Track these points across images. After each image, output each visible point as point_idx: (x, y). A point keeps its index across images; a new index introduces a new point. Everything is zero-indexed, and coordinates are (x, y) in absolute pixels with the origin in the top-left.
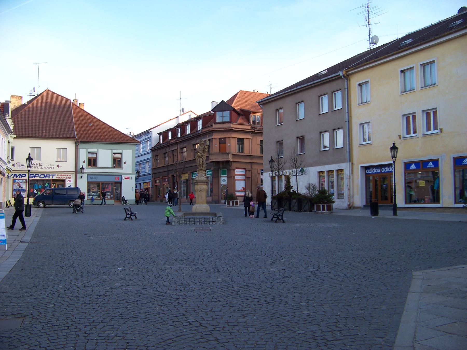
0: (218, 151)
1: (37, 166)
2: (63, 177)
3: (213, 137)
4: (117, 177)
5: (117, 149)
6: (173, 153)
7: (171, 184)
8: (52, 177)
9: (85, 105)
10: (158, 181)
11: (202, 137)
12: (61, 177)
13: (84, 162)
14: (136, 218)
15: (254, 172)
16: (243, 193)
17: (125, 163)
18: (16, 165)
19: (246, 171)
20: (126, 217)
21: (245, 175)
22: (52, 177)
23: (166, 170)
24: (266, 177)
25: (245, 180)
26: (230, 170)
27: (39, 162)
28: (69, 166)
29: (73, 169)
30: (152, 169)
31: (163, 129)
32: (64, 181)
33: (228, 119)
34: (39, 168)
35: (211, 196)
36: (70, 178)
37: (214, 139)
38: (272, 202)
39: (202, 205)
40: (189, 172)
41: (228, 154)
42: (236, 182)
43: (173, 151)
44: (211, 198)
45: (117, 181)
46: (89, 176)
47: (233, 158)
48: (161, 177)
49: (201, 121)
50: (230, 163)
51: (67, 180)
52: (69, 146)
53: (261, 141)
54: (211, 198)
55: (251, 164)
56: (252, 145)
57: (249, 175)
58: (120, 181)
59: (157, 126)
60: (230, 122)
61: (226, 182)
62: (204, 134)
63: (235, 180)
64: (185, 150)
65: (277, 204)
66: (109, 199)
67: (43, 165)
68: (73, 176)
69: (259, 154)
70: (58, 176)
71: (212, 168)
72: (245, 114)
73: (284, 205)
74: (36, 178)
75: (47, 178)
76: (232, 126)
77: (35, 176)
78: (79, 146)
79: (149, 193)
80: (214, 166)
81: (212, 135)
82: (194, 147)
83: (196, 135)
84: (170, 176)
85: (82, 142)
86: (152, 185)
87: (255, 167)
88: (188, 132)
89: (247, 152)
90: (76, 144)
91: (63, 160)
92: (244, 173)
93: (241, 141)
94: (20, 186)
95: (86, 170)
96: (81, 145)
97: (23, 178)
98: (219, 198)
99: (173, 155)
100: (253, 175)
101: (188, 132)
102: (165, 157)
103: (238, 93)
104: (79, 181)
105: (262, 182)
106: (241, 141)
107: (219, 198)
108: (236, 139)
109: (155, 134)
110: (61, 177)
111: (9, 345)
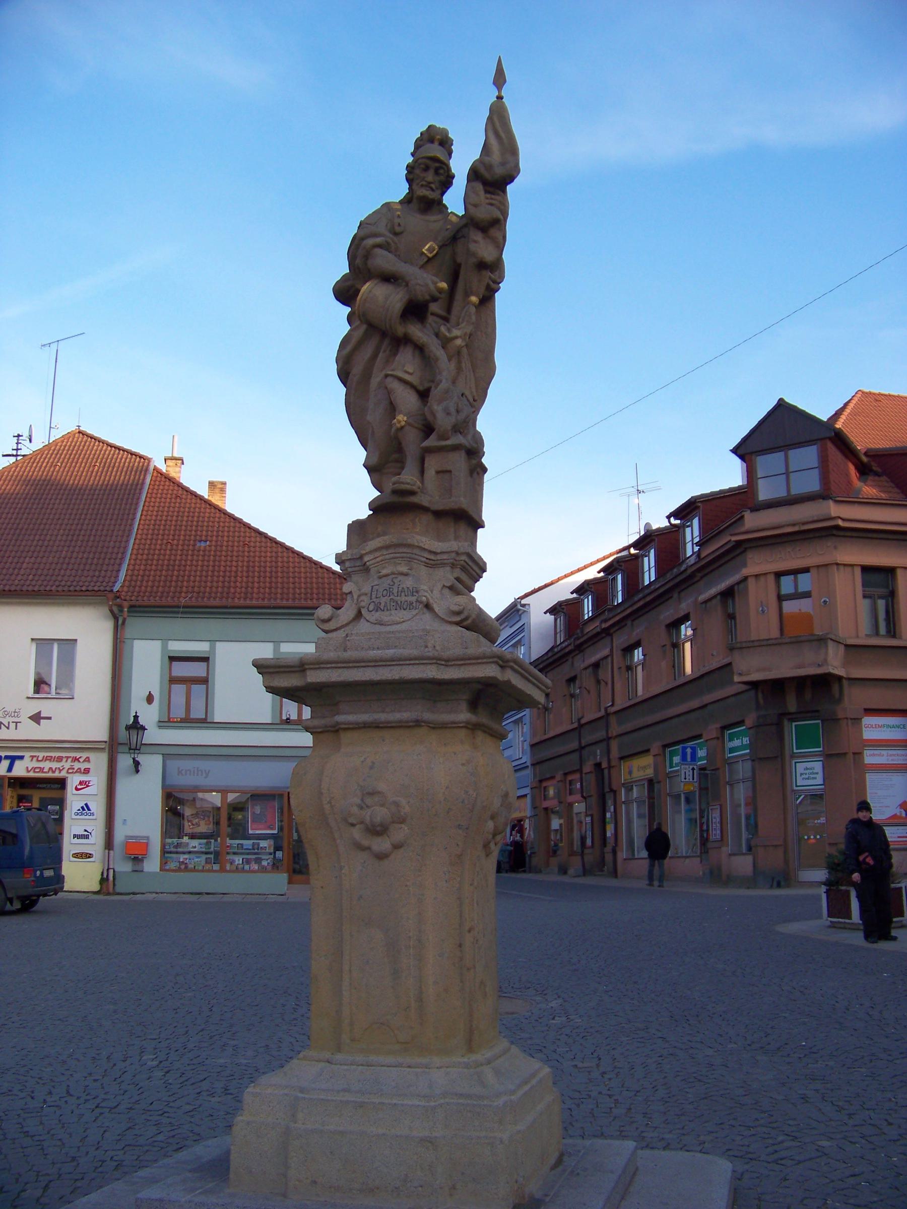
0: (775, 633)
2: (54, 765)
3: (745, 572)
6: (596, 674)
7: (594, 800)
8: (10, 769)
10: (551, 792)
11: (702, 583)
12: (48, 768)
13: (150, 699)
22: (10, 769)
23: (574, 745)
26: (837, 720)
27: (16, 720)
28: (82, 715)
29: (100, 733)
30: (532, 746)
31: (564, 592)
33: (810, 483)
35: (750, 849)
36: (87, 771)
37: (751, 582)
40: (655, 748)
41: (822, 641)
42: (871, 779)
43: (596, 666)
44: (749, 859)
46: (173, 764)
47: (846, 664)
48: (559, 777)
49: (696, 522)
50: (835, 688)
51: (73, 781)
52: (87, 630)
54: (749, 859)
59: (546, 586)
60: (824, 495)
61: (819, 780)
62: (707, 567)
63: (863, 769)
64: (638, 654)
66: (263, 870)
68: (99, 762)
70: (35, 764)
71: (750, 721)
78: (129, 632)
79: (522, 837)
80: (758, 707)
81: (745, 565)
82: (670, 635)
84: (588, 767)
85: (138, 609)
86: (534, 807)
88: (649, 574)
90: (116, 619)
93: (880, 579)
96: (134, 625)
98: (786, 862)
99: (598, 682)
101: (649, 574)
102: (572, 696)
103: (846, 405)
104: (126, 786)
106: (880, 579)
107: (786, 862)
108: (858, 571)
109: (539, 619)
110: (47, 765)
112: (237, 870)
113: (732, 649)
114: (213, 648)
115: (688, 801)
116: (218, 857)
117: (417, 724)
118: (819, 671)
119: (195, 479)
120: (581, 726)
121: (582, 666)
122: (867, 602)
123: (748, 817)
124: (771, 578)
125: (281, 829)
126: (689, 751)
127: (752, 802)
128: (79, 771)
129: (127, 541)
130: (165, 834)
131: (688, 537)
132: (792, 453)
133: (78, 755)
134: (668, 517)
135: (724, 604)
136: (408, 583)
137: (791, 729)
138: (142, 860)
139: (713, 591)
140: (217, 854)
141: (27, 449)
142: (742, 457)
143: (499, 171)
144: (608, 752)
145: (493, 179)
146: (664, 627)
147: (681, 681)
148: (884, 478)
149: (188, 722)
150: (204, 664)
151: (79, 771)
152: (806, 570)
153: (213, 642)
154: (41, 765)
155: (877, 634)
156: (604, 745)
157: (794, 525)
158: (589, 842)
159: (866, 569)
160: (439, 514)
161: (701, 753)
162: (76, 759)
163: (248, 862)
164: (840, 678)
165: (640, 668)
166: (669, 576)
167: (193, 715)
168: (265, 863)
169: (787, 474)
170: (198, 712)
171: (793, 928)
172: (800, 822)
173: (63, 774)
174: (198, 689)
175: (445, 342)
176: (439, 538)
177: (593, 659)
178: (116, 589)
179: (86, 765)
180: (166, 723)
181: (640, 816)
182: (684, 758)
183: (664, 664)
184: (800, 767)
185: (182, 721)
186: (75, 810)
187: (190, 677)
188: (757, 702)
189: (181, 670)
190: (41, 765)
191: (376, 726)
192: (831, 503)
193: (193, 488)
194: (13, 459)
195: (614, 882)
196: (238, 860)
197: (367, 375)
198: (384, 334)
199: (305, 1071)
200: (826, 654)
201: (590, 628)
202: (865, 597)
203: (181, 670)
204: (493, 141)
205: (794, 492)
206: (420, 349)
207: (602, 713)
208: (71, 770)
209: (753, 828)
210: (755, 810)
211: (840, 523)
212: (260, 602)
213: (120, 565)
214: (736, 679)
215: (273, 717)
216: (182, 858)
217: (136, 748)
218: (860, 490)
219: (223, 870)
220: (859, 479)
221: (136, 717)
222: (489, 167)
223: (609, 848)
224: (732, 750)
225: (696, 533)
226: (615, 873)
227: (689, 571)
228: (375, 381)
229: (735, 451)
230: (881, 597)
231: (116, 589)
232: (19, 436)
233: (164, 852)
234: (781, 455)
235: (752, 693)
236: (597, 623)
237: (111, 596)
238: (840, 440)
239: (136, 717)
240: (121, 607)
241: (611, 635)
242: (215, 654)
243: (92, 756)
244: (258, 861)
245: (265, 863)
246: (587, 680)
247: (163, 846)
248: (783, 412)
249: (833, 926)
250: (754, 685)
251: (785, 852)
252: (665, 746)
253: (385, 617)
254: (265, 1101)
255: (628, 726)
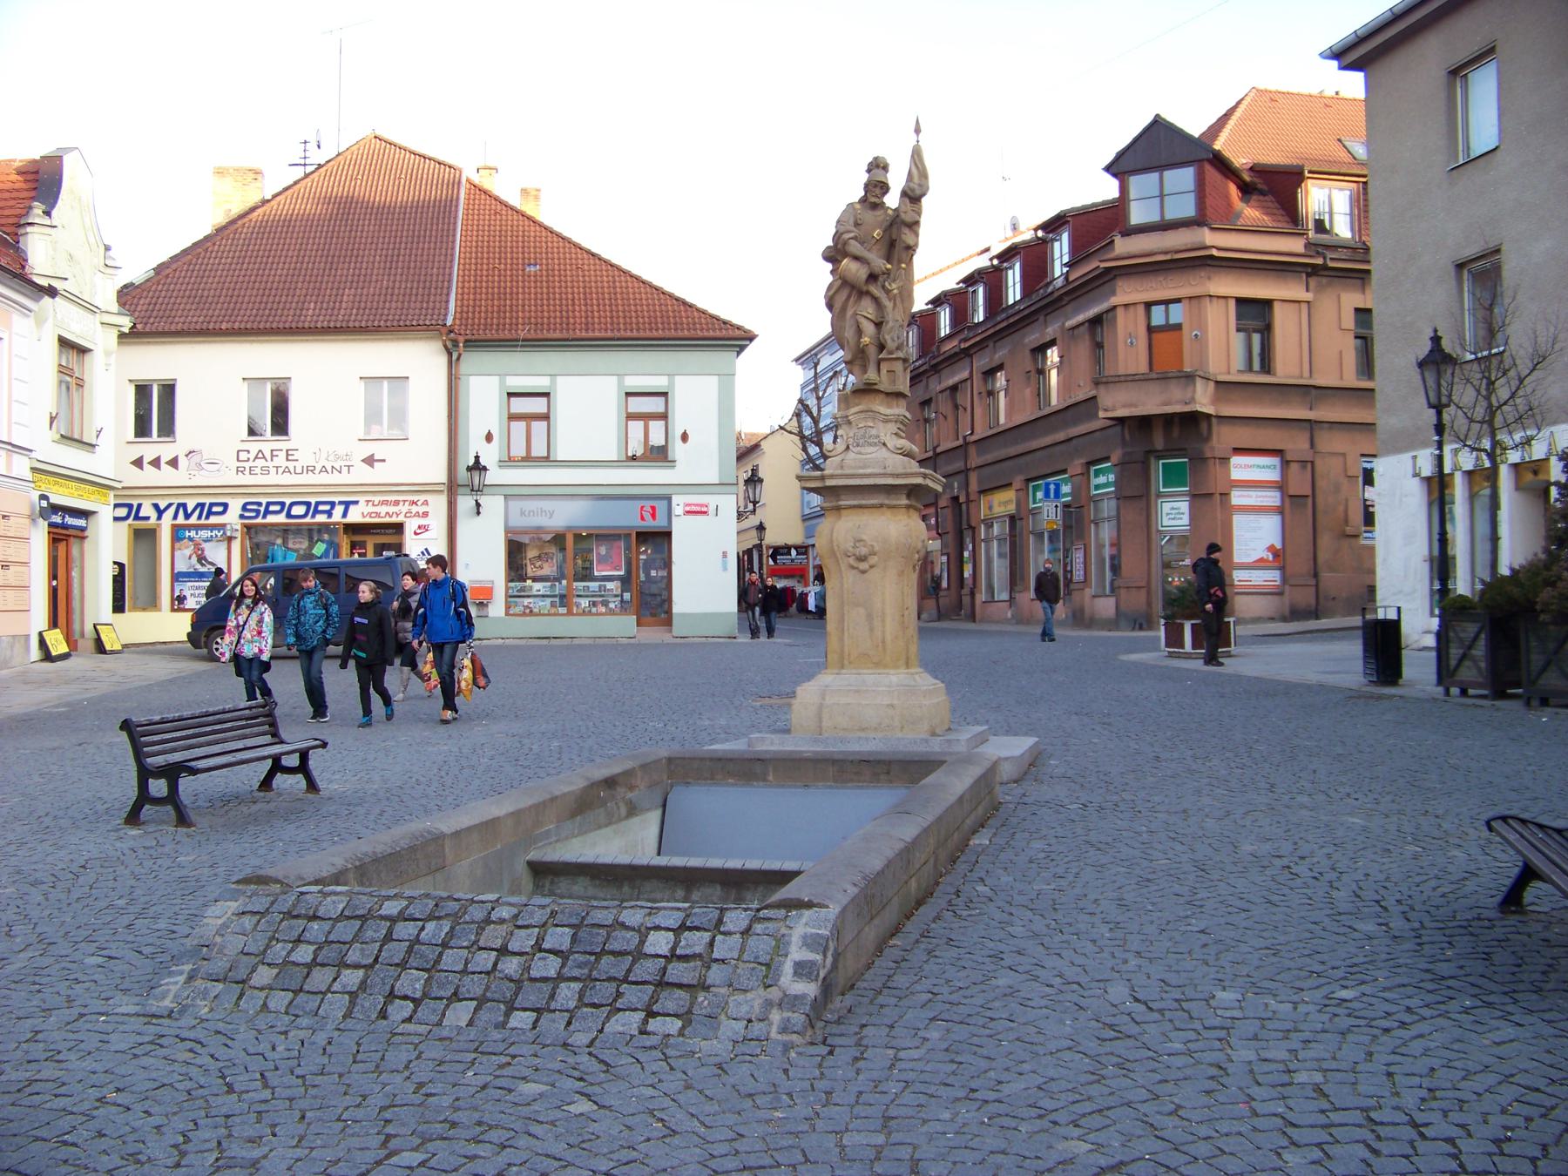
0: (1143, 367)
1: (277, 462)
2: (392, 509)
3: (1114, 301)
4: (648, 504)
5: (645, 370)
6: (953, 398)
7: (950, 538)
8: (345, 515)
9: (543, 195)
11: (1069, 308)
12: (386, 514)
13: (489, 438)
14: (312, 786)
15: (1328, 468)
16: (1271, 577)
17: (685, 437)
18: (182, 462)
19: (1285, 464)
20: (144, 798)
21: (1281, 486)
22: (345, 515)
24: (1397, 488)
25: (1280, 510)
26: (1204, 460)
29: (442, 477)
32: (399, 528)
33: (1184, 207)
34: (287, 471)
35: (1113, 589)
36: (426, 514)
37: (1120, 312)
38: (1441, 636)
39: (870, 677)
40: (1018, 482)
41: (1190, 378)
42: (1238, 520)
43: (954, 389)
44: (1112, 601)
45: (649, 524)
46: (515, 505)
47: (1216, 400)
49: (1065, 237)
50: (1204, 426)
51: (410, 526)
52: (418, 362)
53: (1363, 314)
54: (1112, 601)
55: (1318, 434)
56: (1313, 336)
57: (1299, 485)
58: (659, 523)
61: (1185, 520)
62: (1076, 292)
63: (1229, 510)
64: (1001, 379)
65: (1480, 651)
66: (611, 612)
67: (304, 458)
68: (438, 504)
69: (1351, 379)
70: (371, 509)
71: (1116, 456)
72: (1277, 187)
73: (1537, 660)
74: (271, 519)
75: (321, 518)
76: (1209, 237)
77: (267, 512)
80: (1124, 443)
81: (1113, 293)
82: (1035, 360)
83: (1045, 302)
85: (474, 344)
87: (1331, 443)
88: (1014, 293)
89: (1287, 368)
90: (450, 354)
91: (396, 433)
92: (1274, 475)
93: (1255, 313)
94: (202, 559)
95: (494, 476)
96: (472, 361)
97: (213, 520)
99: (956, 407)
100: (1320, 483)
101: (1014, 293)
102: (927, 421)
103: (1239, 103)
105: (1369, 519)
106: (1255, 313)
108: (1232, 303)
110: (383, 510)
111: (510, 1091)
112: (584, 613)
113: (1097, 383)
114: (553, 383)
115: (1051, 540)
116: (564, 599)
117: (881, 506)
118: (1187, 409)
119: (506, 189)
120: (937, 455)
121: (939, 388)
122: (1242, 335)
123: (1112, 558)
124: (1141, 310)
125: (629, 571)
126: (1052, 487)
127: (1116, 544)
128: (417, 515)
129: (451, 268)
130: (510, 579)
131: (1057, 254)
132: (1168, 174)
133: (415, 498)
134: (1036, 230)
135: (1093, 333)
136: (874, 432)
137: (1158, 468)
139: (1081, 318)
140: (562, 597)
141: (318, 157)
142: (1115, 175)
143: (918, 192)
144: (967, 485)
145: (913, 196)
146: (1027, 353)
147: (1047, 411)
148: (1270, 198)
149: (529, 459)
150: (545, 400)
151: (417, 515)
152: (1178, 301)
155: (1250, 369)
156: (961, 477)
157: (1166, 253)
158: (944, 584)
159: (1241, 302)
160: (888, 394)
161: (1066, 489)
163: (594, 604)
164: (1208, 416)
165: (1002, 394)
166: (1035, 298)
167: (534, 454)
168: (612, 606)
169: (1162, 196)
170: (539, 450)
171: (1134, 657)
172: (1167, 565)
173: (400, 519)
174: (539, 427)
175: (888, 292)
176: (889, 407)
177: (951, 382)
178: (449, 322)
179: (424, 509)
180: (508, 461)
181: (1000, 555)
182: (1047, 495)
183: (1028, 391)
184: (1167, 507)
185: (523, 459)
187: (531, 412)
188: (1123, 438)
189: (520, 406)
191: (860, 507)
192: (1206, 230)
193: (504, 197)
195: (970, 626)
196: (584, 603)
197: (844, 309)
198: (853, 287)
199: (826, 679)
200: (1194, 391)
201: (947, 347)
202: (1238, 330)
203: (520, 406)
204: (915, 171)
205: (1169, 216)
206: (876, 300)
207: (961, 442)
208: (408, 514)
209: (1115, 569)
210: (1119, 551)
211: (1215, 252)
212: (603, 334)
213: (448, 294)
214: (1101, 414)
216: (526, 601)
218: (1239, 215)
219: (570, 613)
220: (1241, 200)
221: (477, 457)
222: (913, 190)
223: (966, 591)
224: (1097, 487)
225: (1066, 249)
226: (972, 617)
227: (1056, 295)
228: (850, 313)
229: (1108, 169)
230: (1255, 331)
231: (449, 322)
233: (508, 596)
234: (1155, 176)
235: (1118, 429)
236: (955, 343)
237: (444, 330)
238: (1221, 163)
239: (477, 457)
240: (455, 343)
241: (971, 356)
244: (605, 603)
245: (612, 606)
246: (944, 406)
247: (507, 589)
248: (1158, 127)
249: (1171, 655)
250: (1121, 421)
251: (1149, 593)
252: (1028, 480)
253: (862, 450)
254: (807, 694)
255: (989, 457)
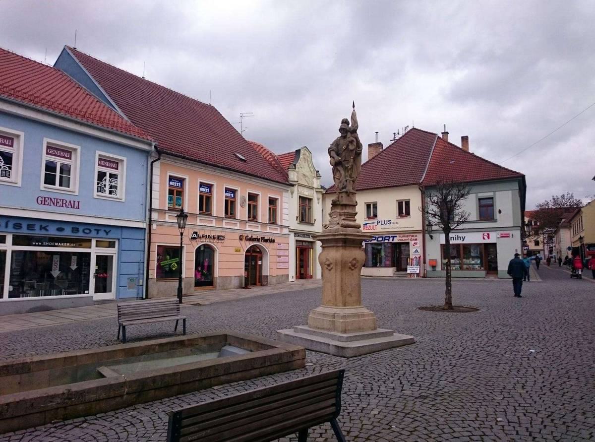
8: (393, 240)
12: (404, 239)
22: (393, 240)
36: (416, 240)
68: (420, 237)
70: (400, 238)
110: (404, 238)
114: (495, 194)
133: (413, 235)
138: (435, 267)
150: (491, 200)
151: (414, 240)
153: (494, 192)
154: (402, 238)
162: (413, 236)
173: (409, 241)
179: (416, 238)
186: (413, 252)
190: (402, 238)
194: (393, 141)
208: (411, 240)
215: (477, 218)
217: (430, 232)
232: (395, 133)
242: (495, 197)
243: (418, 235)
